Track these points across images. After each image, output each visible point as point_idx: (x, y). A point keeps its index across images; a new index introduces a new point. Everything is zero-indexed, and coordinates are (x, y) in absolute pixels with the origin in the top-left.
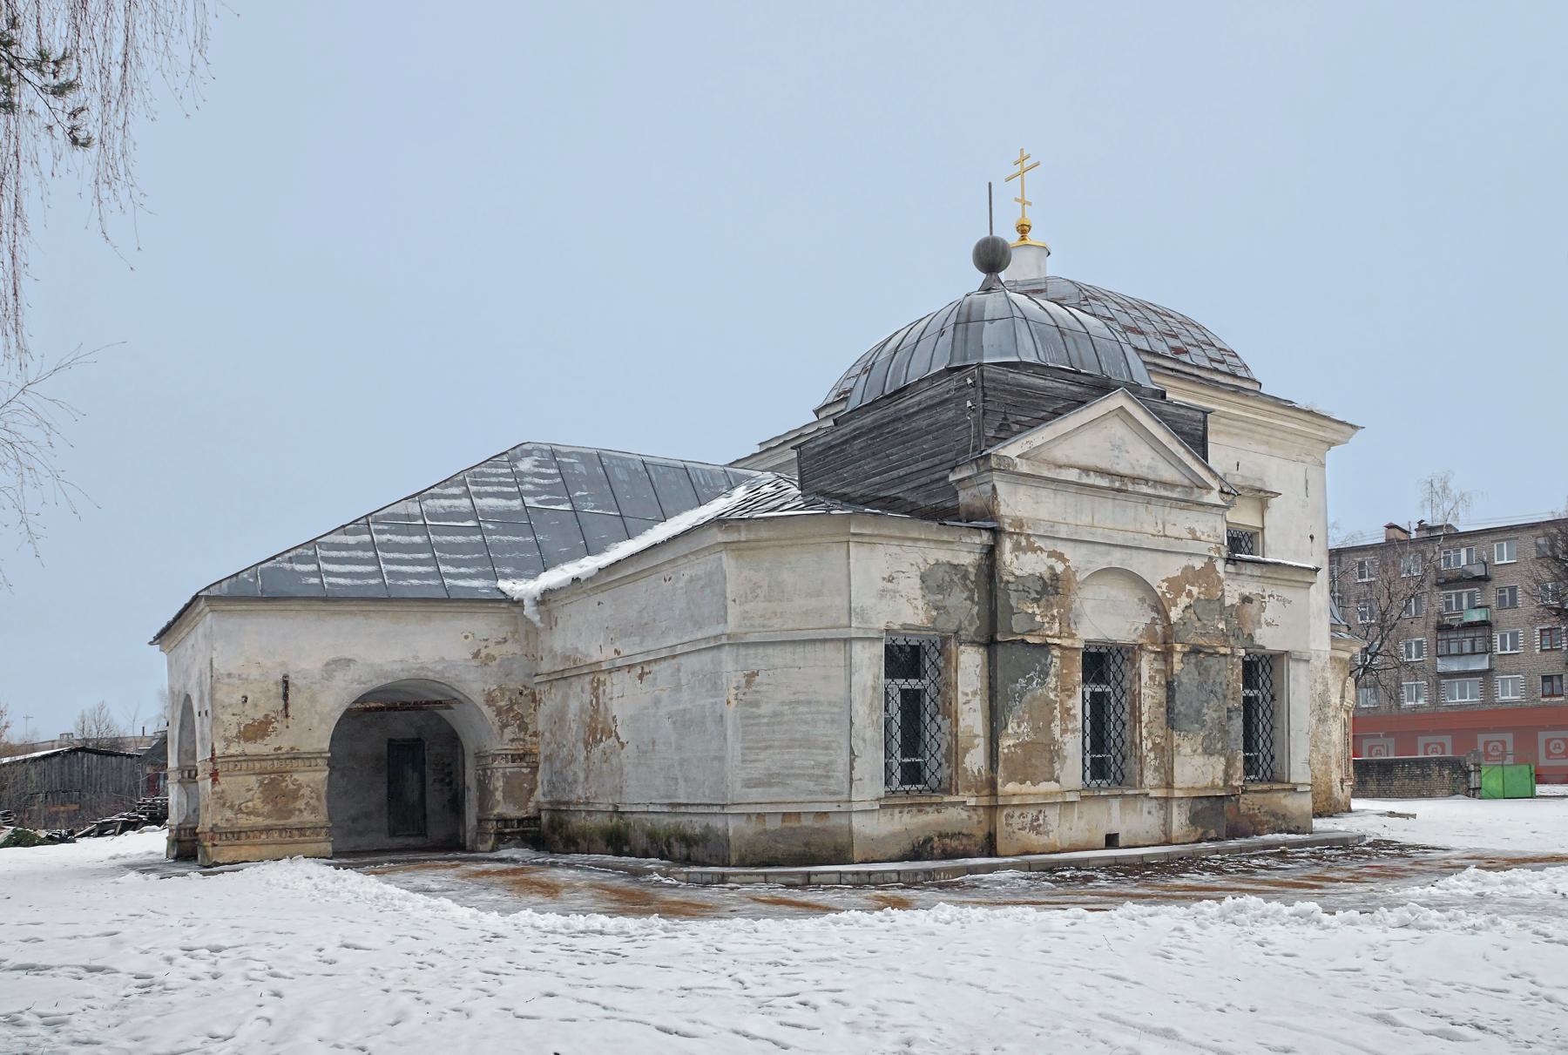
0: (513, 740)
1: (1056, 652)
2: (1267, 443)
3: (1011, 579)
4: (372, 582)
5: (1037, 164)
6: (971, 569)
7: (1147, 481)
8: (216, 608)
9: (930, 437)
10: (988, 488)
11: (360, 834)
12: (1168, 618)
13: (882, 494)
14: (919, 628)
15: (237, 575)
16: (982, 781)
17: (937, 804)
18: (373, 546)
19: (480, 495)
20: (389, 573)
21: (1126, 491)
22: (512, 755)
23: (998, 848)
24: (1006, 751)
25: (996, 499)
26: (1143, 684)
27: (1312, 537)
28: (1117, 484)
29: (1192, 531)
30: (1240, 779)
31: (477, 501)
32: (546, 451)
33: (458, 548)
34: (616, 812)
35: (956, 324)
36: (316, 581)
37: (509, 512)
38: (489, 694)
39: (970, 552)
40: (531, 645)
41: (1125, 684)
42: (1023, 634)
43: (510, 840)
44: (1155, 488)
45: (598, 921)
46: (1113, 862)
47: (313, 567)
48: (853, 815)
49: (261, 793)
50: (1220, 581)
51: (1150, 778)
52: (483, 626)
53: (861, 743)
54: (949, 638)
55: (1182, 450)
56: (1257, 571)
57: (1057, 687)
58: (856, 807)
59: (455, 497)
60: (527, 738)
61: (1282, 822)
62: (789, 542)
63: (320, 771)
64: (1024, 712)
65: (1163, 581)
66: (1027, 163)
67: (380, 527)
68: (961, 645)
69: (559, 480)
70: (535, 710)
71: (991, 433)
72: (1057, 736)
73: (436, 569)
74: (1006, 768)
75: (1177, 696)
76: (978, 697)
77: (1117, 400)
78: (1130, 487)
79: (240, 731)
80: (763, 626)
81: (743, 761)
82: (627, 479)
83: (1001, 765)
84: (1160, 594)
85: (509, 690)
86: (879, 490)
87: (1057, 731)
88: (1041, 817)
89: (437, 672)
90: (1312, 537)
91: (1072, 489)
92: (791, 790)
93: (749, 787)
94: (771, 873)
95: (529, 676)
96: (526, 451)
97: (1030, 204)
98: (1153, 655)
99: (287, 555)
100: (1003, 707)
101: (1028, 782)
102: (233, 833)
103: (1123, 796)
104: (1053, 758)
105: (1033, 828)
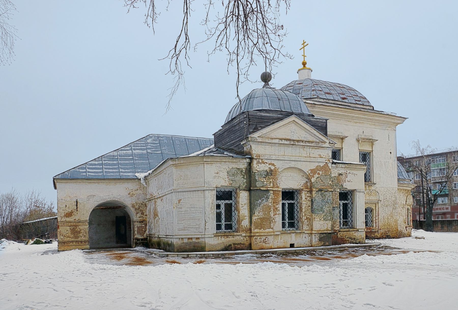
0: (140, 217)
1: (272, 192)
2: (374, 125)
3: (256, 172)
4: (100, 174)
5: (308, 44)
6: (243, 169)
7: (303, 141)
8: (58, 181)
9: (239, 132)
10: (249, 146)
11: (108, 243)
12: (311, 181)
13: (230, 148)
14: (226, 186)
15: (64, 173)
16: (247, 229)
17: (233, 235)
18: (118, 164)
19: (135, 149)
20: (105, 172)
21: (295, 145)
22: (140, 221)
23: (252, 248)
24: (255, 220)
25: (251, 149)
26: (303, 200)
27: (391, 153)
28: (292, 143)
29: (320, 155)
30: (338, 228)
31: (134, 151)
32: (156, 136)
33: (126, 164)
34: (158, 237)
35: (247, 99)
36: (85, 174)
37: (142, 154)
38: (133, 204)
39: (243, 165)
40: (145, 191)
41: (298, 200)
42: (260, 187)
43: (139, 245)
44: (306, 143)
45: (110, 266)
46: (285, 252)
47: (85, 170)
48: (206, 239)
49: (70, 231)
50: (330, 169)
51: (305, 227)
52: (131, 186)
53: (208, 219)
54: (237, 189)
55: (315, 132)
56: (343, 166)
57: (272, 202)
58: (206, 236)
59: (128, 150)
60: (144, 216)
61: (353, 240)
62: (189, 164)
63: (86, 225)
64: (261, 209)
65: (309, 170)
66: (305, 44)
67: (105, 159)
68: (240, 190)
69: (159, 144)
70: (146, 209)
71: (251, 130)
72: (272, 216)
73: (119, 170)
74: (254, 225)
75: (314, 204)
76: (246, 205)
77: (293, 118)
78: (297, 143)
79: (65, 215)
80: (183, 187)
81: (178, 224)
82: (179, 143)
83: (253, 224)
84: (308, 174)
85: (138, 203)
86: (229, 147)
87: (272, 214)
88: (267, 239)
89: (118, 199)
90: (391, 153)
91: (277, 145)
92: (190, 231)
93: (179, 231)
94: (179, 254)
95: (144, 199)
96: (150, 137)
97: (306, 56)
98: (306, 192)
99: (78, 167)
100: (254, 208)
101: (262, 229)
102: (63, 242)
103: (296, 233)
104: (271, 222)
105: (264, 242)
